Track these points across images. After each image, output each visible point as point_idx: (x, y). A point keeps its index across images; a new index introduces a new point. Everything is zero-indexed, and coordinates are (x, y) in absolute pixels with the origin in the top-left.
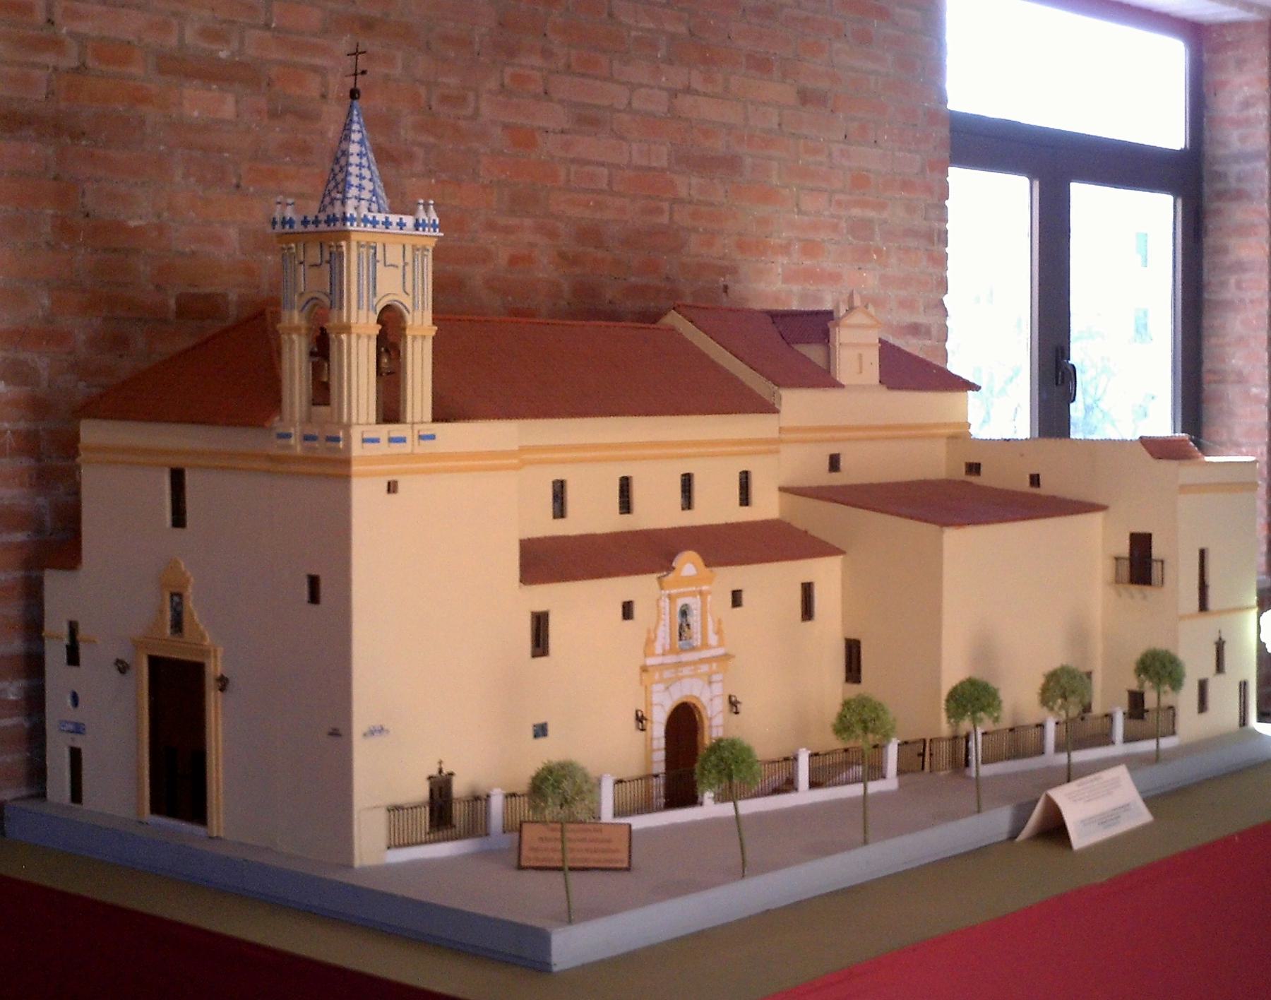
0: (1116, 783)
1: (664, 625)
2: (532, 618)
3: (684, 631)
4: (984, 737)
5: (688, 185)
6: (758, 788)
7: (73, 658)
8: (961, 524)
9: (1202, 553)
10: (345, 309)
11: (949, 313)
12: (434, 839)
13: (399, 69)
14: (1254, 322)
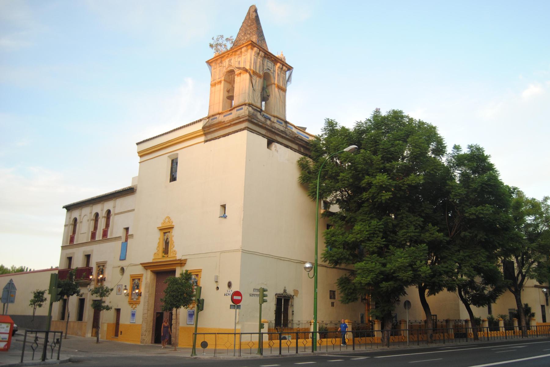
0: (276, 147)
1: (334, 346)
2: (78, 300)
3: (221, 62)
4: (213, 88)
5: (331, 181)
7: (121, 334)
8: (419, 291)
9: (173, 178)
10: (253, 62)
11: (252, 5)
12: (529, 270)
13: (366, 180)
14: (134, 292)
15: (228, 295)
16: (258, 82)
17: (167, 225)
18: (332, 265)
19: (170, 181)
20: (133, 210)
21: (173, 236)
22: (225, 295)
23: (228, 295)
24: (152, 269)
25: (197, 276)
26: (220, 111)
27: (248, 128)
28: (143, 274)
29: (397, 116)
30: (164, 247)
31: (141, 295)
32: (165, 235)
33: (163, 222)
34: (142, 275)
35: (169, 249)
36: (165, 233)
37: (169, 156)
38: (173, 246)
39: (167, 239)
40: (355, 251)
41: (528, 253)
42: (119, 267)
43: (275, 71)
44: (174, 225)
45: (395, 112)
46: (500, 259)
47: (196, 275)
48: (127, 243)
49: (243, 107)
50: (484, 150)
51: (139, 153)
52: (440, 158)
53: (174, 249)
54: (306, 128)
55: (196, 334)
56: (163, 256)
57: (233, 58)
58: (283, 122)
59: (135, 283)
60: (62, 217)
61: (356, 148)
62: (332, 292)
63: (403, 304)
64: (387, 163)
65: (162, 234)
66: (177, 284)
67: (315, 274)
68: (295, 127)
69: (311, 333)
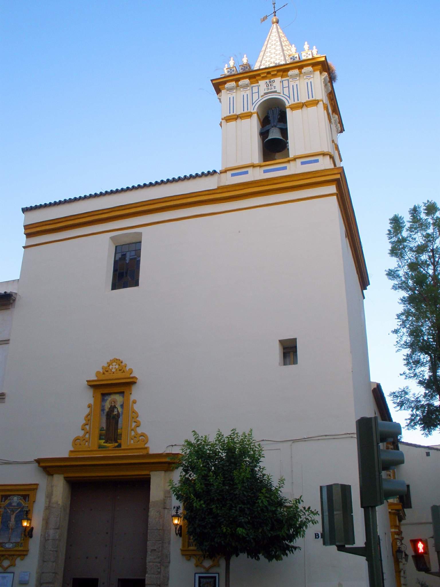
17: (116, 376)
24: (66, 475)
25: (25, 499)
28: (37, 485)
30: (104, 426)
31: (31, 536)
32: (103, 400)
34: (33, 488)
36: (103, 395)
37: (112, 238)
47: (22, 496)
49: (320, 158)
51: (26, 227)
56: (100, 447)
59: (10, 504)
65: (99, 397)
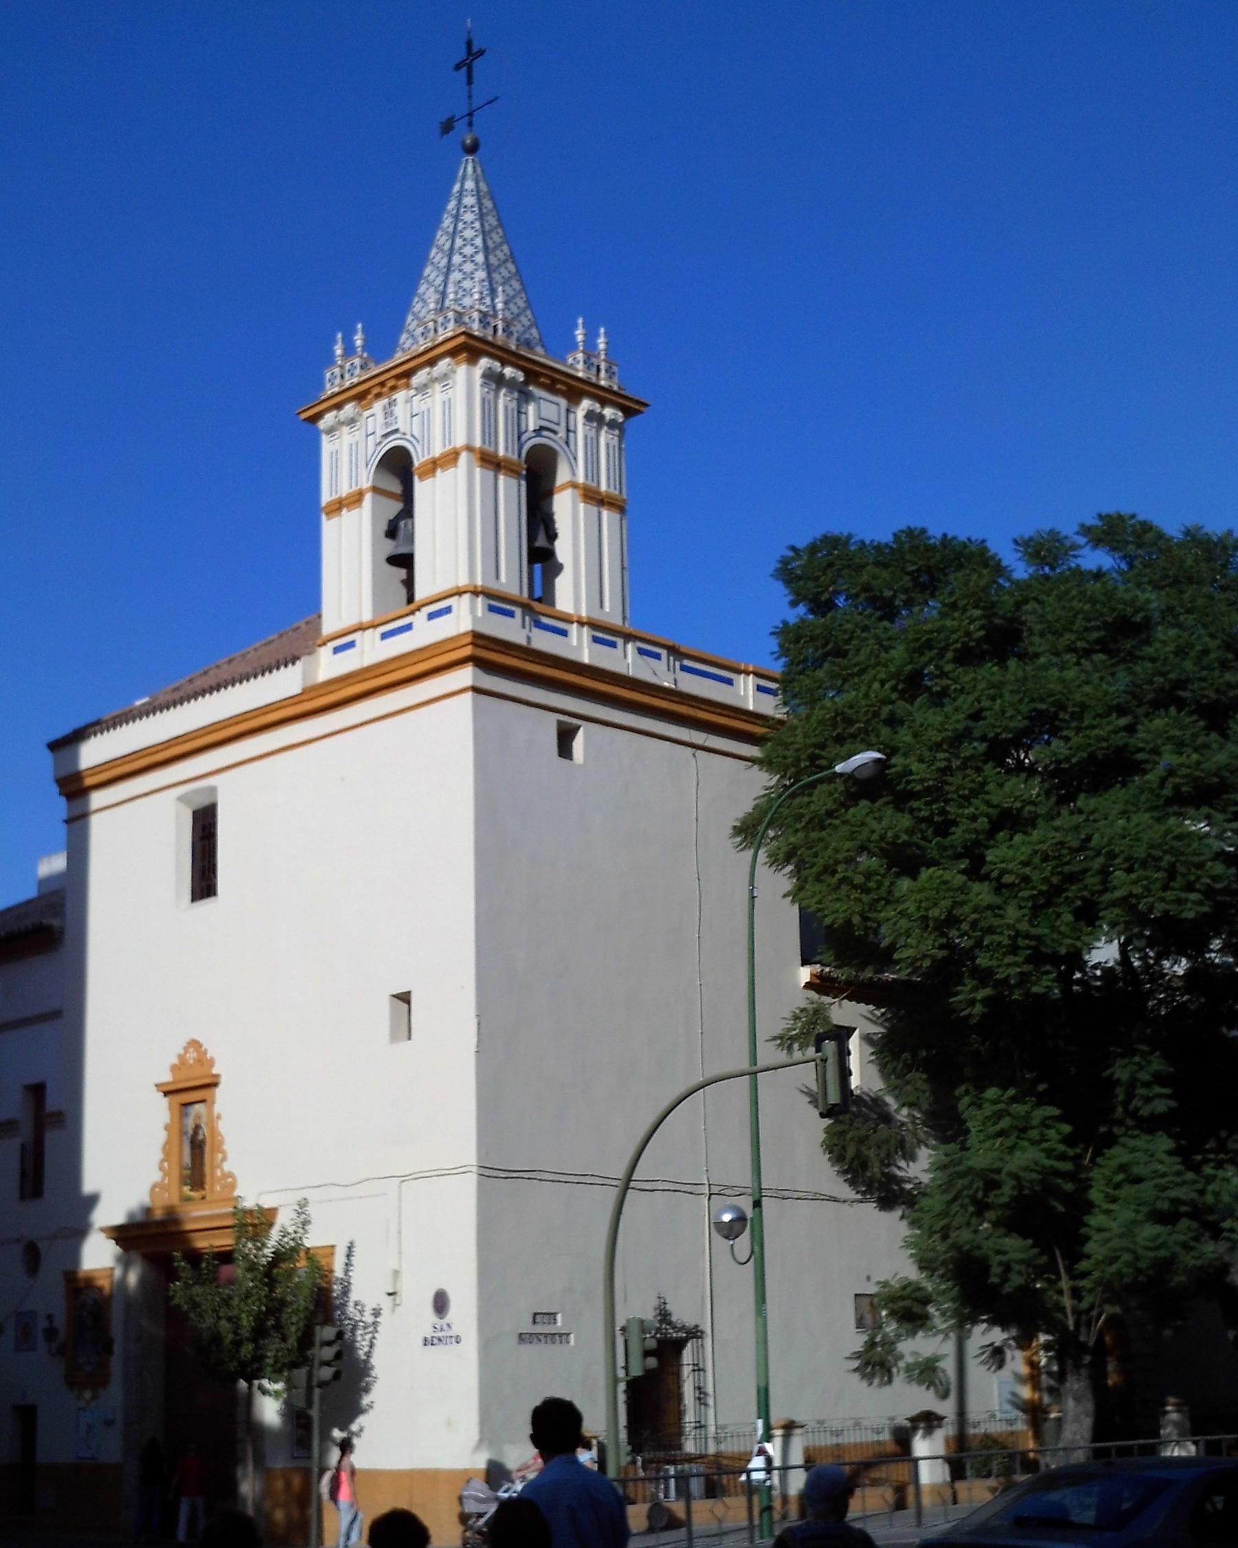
6: (1184, 784)
15: (436, 1341)
16: (510, 491)
18: (1122, 916)
19: (194, 899)
20: (496, 98)
21: (219, 1117)
22: (426, 1342)
23: (436, 1341)
26: (367, 617)
27: (842, 717)
29: (832, 542)
33: (175, 1061)
35: (207, 1169)
37: (181, 799)
38: (220, 1156)
39: (197, 1128)
40: (1141, 563)
41: (1047, 1412)
42: (18, 1240)
43: (575, 432)
44: (217, 1076)
45: (910, 532)
46: (1213, 955)
48: (761, 1212)
50: (774, 868)
52: (1075, 556)
53: (227, 1167)
54: (409, 992)
55: (756, 1073)
57: (400, 396)
58: (664, 653)
60: (160, 1110)
61: (878, 761)
62: (866, 1301)
63: (1136, 1187)
64: (920, 657)
66: (948, 890)
67: (756, 1248)
68: (725, 1458)
69: (673, 1480)
